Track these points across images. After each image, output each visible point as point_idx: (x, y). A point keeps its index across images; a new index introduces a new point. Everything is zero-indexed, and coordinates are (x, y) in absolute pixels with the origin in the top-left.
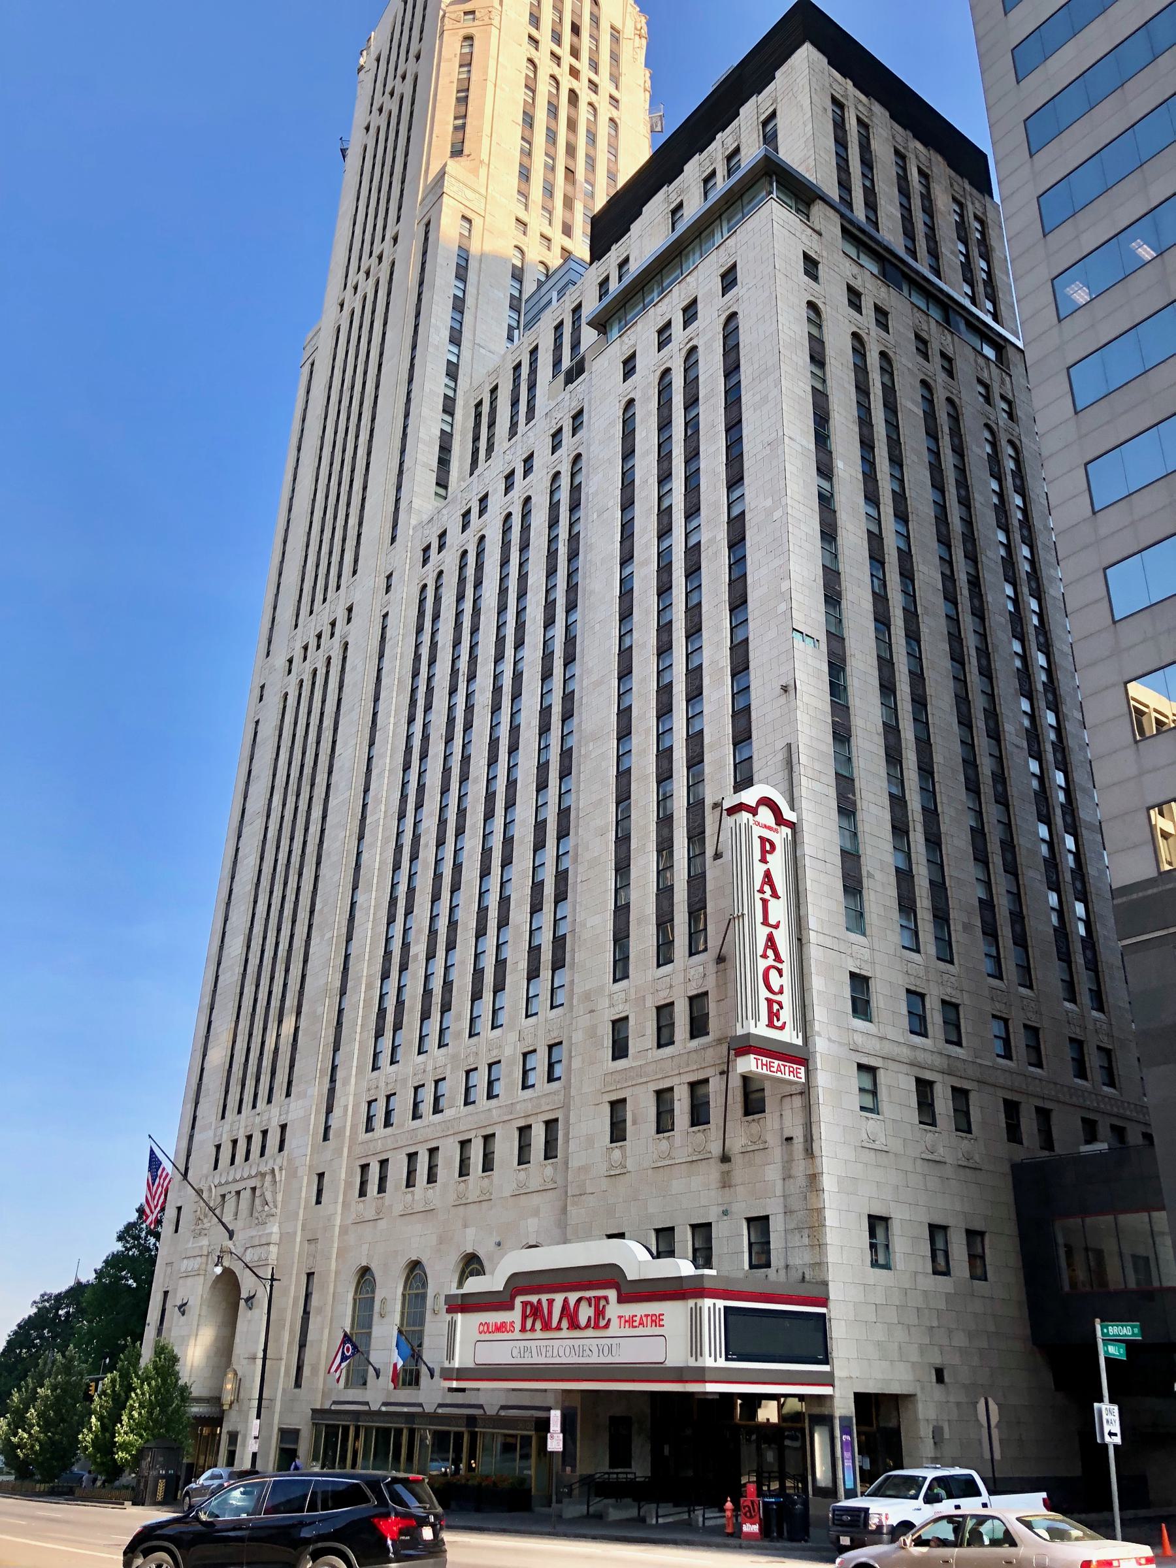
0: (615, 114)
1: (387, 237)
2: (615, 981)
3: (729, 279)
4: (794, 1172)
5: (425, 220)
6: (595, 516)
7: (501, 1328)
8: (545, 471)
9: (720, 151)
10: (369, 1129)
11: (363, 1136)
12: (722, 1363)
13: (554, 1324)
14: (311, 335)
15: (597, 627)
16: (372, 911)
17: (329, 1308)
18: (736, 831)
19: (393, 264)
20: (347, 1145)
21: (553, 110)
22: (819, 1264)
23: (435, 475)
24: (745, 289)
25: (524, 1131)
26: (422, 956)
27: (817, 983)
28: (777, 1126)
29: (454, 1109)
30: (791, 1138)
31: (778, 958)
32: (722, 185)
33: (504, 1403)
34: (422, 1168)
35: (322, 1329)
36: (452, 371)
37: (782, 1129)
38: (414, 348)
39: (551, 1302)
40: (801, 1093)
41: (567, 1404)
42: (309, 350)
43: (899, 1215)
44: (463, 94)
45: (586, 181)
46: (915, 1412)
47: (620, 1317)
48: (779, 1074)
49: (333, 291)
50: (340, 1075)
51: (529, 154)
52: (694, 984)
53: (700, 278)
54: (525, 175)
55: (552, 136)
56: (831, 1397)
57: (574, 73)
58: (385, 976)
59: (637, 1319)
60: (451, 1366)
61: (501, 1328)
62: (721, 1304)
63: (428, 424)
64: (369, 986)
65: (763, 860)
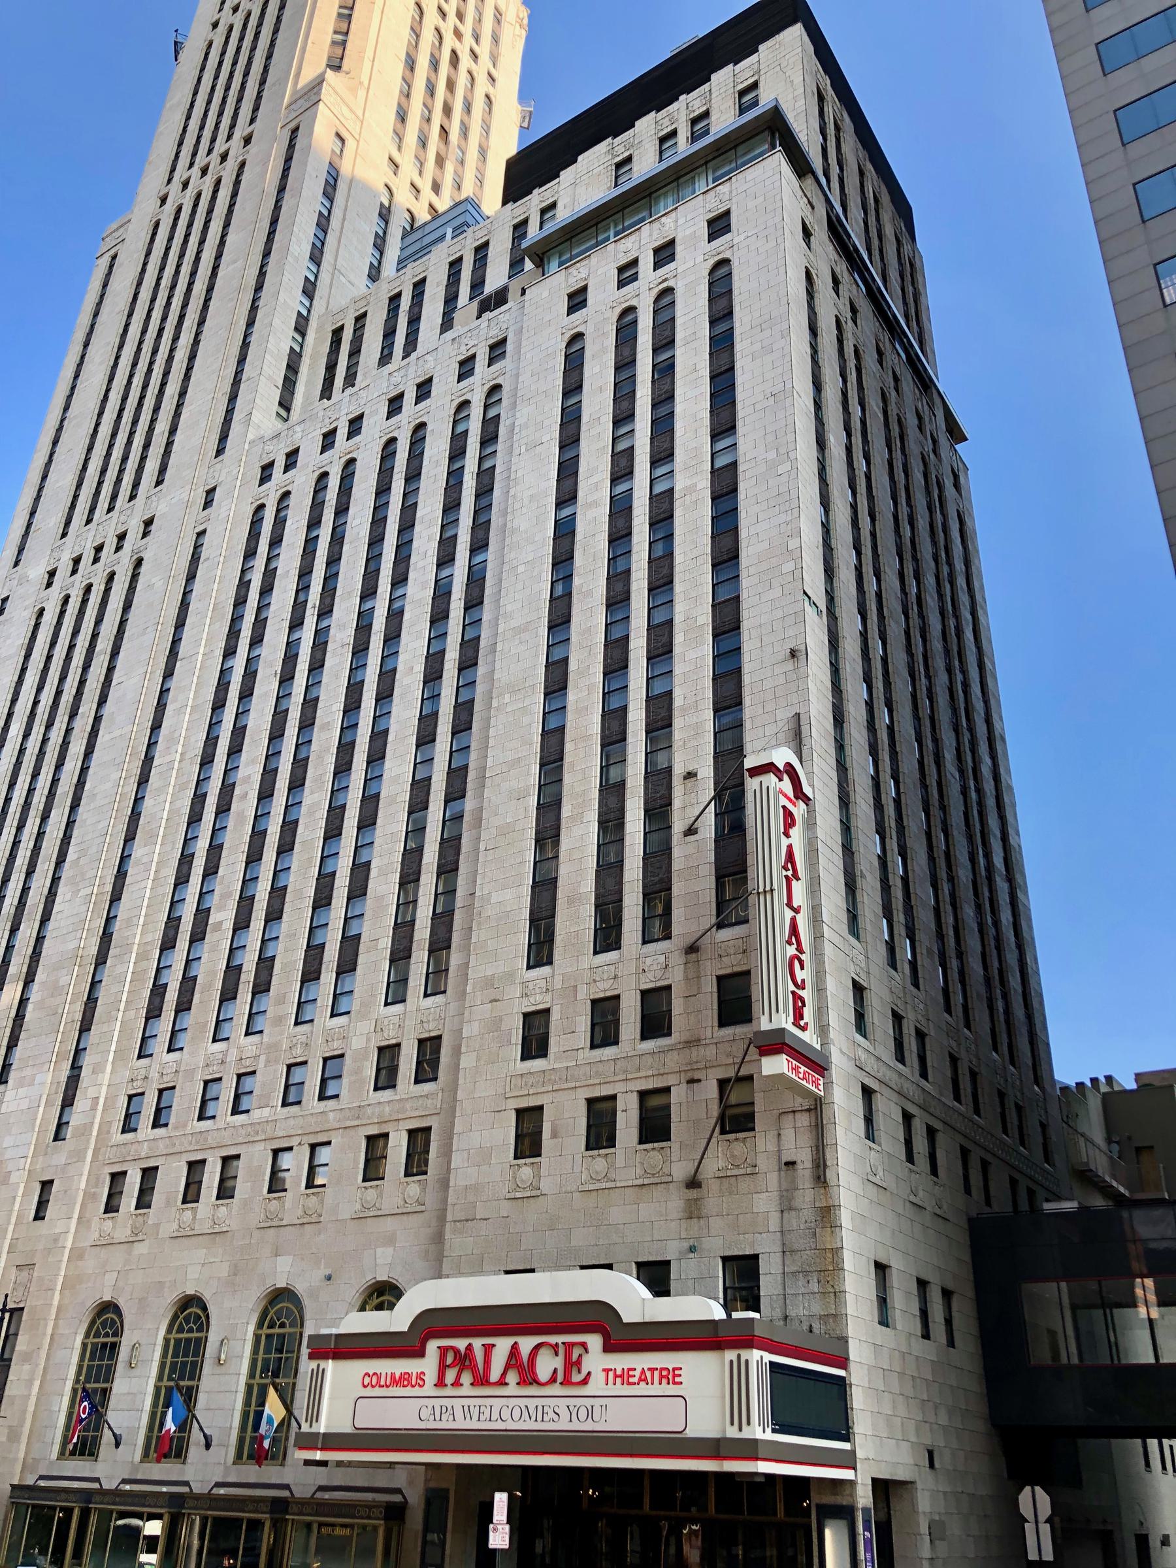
0: (491, 91)
1: (215, 151)
2: (529, 967)
3: (719, 225)
4: (797, 1203)
5: (292, 125)
6: (523, 449)
7: (403, 1380)
8: (449, 398)
9: (683, 112)
10: (128, 1127)
11: (118, 1137)
12: (769, 1436)
13: (495, 1376)
14: (114, 226)
15: (521, 569)
16: (153, 868)
17: (43, 1354)
18: (764, 791)
19: (243, 165)
20: (92, 1146)
21: (435, 65)
22: (835, 1316)
23: (279, 392)
24: (742, 237)
25: (195, 1167)
26: (229, 925)
27: (831, 984)
28: (772, 1147)
29: (266, 1109)
30: (794, 1163)
31: (800, 949)
32: (683, 147)
33: (324, 1483)
34: (211, 1180)
35: (30, 1382)
36: (309, 290)
37: (779, 1151)
38: (267, 254)
39: (488, 1349)
40: (809, 1110)
41: (432, 1485)
42: (110, 242)
43: (896, 1263)
44: (346, 12)
45: (459, 147)
46: (913, 1505)
47: (607, 1371)
48: (804, 1082)
49: (153, 180)
50: (87, 1061)
51: (408, 96)
52: (650, 976)
53: (684, 220)
54: (402, 117)
55: (431, 90)
56: (852, 1483)
57: (458, 34)
58: (168, 944)
59: (637, 1373)
60: (313, 1430)
61: (403, 1380)
62: (768, 1357)
63: (274, 340)
64: (142, 956)
65: (787, 835)
